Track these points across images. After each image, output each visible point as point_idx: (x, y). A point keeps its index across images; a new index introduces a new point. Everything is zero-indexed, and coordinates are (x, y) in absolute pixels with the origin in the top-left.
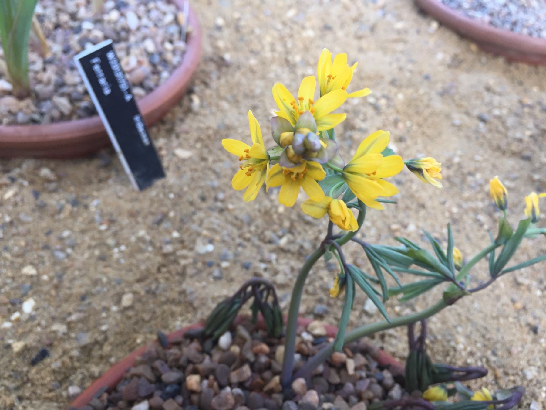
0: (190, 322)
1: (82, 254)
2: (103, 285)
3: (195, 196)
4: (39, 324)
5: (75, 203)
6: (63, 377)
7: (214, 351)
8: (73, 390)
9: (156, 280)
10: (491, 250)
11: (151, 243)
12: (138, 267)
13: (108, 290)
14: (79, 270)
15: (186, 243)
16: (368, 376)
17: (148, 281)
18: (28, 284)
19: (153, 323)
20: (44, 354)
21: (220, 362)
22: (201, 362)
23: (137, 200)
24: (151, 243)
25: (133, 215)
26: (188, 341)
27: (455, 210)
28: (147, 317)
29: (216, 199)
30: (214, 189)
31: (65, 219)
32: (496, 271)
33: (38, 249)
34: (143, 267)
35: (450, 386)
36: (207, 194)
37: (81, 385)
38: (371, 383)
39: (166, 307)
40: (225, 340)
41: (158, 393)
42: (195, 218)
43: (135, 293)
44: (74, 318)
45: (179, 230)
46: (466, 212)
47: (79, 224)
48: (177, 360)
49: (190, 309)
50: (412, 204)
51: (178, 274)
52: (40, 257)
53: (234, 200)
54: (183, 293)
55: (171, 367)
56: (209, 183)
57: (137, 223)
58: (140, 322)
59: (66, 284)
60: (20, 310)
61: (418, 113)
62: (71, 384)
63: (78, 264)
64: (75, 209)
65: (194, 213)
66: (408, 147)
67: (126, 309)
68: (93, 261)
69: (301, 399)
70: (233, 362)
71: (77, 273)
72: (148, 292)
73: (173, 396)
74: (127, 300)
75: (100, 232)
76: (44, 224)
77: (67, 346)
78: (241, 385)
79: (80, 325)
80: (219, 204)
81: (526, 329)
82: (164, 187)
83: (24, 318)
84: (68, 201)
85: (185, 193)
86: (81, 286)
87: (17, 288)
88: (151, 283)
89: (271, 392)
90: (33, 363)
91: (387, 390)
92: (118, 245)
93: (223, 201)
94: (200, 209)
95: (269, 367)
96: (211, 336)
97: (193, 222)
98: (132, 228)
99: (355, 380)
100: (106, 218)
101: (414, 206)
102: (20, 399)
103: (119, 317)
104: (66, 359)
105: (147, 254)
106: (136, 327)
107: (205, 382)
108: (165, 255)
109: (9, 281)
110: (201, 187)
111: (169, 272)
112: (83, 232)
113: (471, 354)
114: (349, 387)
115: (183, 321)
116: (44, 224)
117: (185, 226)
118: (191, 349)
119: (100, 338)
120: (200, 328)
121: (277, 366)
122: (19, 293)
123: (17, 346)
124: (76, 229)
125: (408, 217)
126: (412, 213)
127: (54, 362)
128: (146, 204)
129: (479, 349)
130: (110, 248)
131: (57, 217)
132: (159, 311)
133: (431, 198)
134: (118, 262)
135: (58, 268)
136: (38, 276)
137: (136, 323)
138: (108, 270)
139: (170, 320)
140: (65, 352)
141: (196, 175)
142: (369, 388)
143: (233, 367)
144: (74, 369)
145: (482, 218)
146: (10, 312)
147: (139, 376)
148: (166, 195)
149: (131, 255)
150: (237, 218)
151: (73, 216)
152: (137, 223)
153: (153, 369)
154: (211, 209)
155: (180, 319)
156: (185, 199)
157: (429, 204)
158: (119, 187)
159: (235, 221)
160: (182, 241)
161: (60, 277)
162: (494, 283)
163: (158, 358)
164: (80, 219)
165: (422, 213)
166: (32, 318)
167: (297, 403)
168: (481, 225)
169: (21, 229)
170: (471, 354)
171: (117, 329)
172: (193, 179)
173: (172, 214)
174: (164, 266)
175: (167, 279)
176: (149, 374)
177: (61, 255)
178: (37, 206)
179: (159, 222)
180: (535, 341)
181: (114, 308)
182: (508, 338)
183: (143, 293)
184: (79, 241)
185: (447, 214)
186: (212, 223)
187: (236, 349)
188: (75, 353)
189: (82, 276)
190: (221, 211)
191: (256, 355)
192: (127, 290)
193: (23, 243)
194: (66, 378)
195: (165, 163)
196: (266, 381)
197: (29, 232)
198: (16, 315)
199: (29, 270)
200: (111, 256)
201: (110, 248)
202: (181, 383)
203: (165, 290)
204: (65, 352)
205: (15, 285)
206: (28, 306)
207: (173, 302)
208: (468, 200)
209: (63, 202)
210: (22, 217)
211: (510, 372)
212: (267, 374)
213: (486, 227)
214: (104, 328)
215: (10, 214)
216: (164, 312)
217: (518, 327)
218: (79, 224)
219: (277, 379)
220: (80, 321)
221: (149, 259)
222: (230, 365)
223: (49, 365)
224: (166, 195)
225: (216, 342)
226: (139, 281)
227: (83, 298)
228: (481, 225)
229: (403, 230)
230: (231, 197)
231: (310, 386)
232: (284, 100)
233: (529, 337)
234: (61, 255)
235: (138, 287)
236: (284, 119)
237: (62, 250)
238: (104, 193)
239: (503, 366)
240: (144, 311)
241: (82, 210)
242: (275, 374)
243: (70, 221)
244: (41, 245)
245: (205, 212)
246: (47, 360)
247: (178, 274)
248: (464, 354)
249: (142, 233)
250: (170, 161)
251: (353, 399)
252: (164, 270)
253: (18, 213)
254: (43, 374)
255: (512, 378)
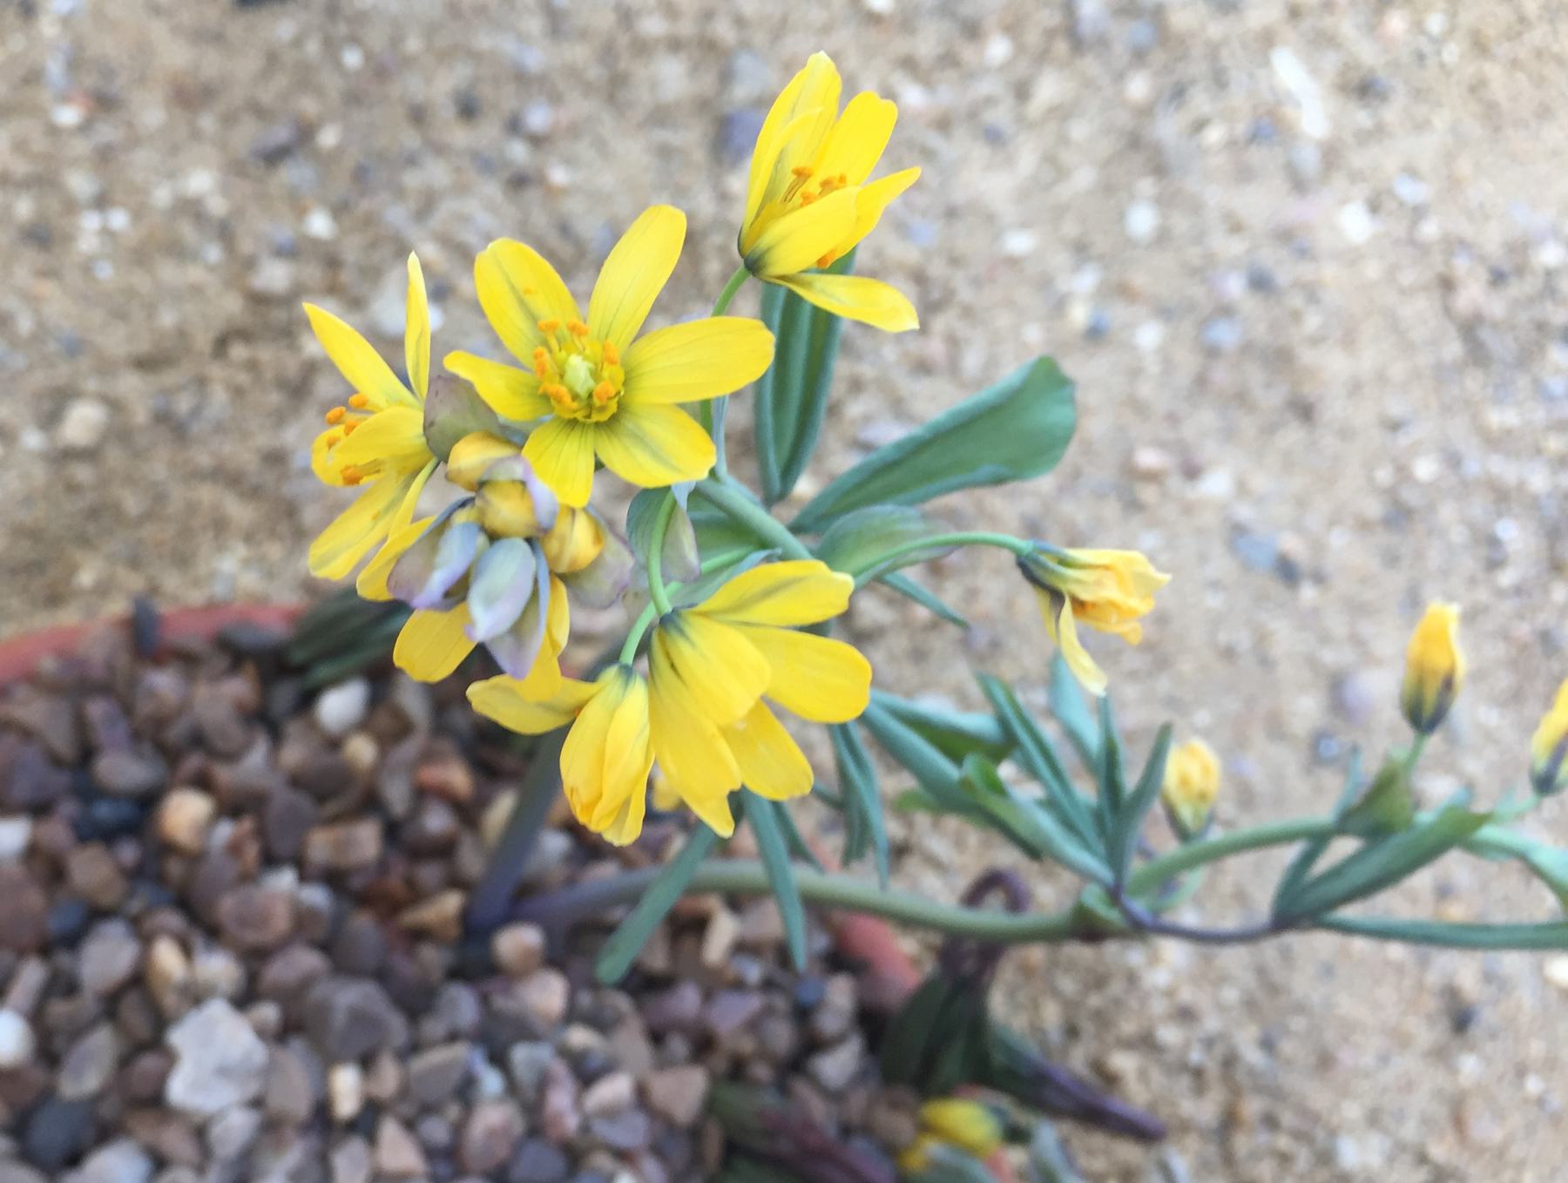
0: (270, 575)
7: (293, 729)
9: (201, 382)
11: (225, 232)
12: (151, 309)
13: (30, 368)
15: (346, 277)
16: (768, 985)
17: (170, 378)
19: (149, 532)
21: (297, 781)
22: (232, 757)
23: (217, 38)
25: (190, 97)
26: (222, 662)
28: (132, 503)
29: (514, 126)
30: (522, 79)
34: (168, 319)
35: (1023, 1117)
36: (486, 91)
38: (768, 1011)
39: (207, 494)
40: (340, 704)
41: (68, 808)
42: (412, 180)
43: (114, 405)
45: (339, 210)
46: (1465, 488)
48: (160, 722)
49: (284, 528)
50: (1268, 386)
51: (282, 383)
53: (583, 149)
54: (276, 458)
55: (136, 736)
56: (508, 46)
57: (196, 135)
58: (101, 516)
65: (412, 161)
66: (1379, 132)
69: (507, 991)
70: (334, 791)
72: (164, 418)
73: (108, 836)
74: (83, 421)
75: (53, 131)
78: (334, 878)
80: (519, 152)
81: (1431, 1003)
85: (408, 62)
88: (181, 388)
89: (419, 935)
91: (812, 1044)
92: (102, 202)
93: (537, 141)
94: (440, 150)
95: (443, 850)
96: (301, 670)
97: (400, 193)
98: (174, 150)
99: (716, 984)
100: (90, 80)
101: (1270, 398)
105: (195, 274)
106: (91, 529)
107: (225, 831)
108: (259, 300)
110: (475, 56)
111: (252, 366)
113: (1186, 1015)
114: (686, 1000)
117: (365, 205)
118: (221, 698)
120: (274, 629)
121: (471, 861)
126: (1248, 425)
128: (246, 66)
129: (1221, 1008)
130: (71, 207)
132: (178, 495)
133: (1355, 388)
134: (87, 268)
137: (94, 513)
138: (47, 288)
142: (754, 1025)
143: (332, 808)
145: (1514, 534)
148: (331, 47)
149: (140, 255)
150: (565, 229)
152: (196, 135)
153: (81, 725)
154: (486, 164)
155: (241, 550)
157: (1334, 408)
159: (553, 240)
163: (103, 689)
165: (1292, 435)
168: (1495, 561)
170: (1186, 1015)
171: (25, 516)
173: (328, 138)
175: (238, 392)
176: (61, 739)
179: (274, 157)
180: (1441, 1055)
181: (33, 439)
182: (1348, 1005)
183: (140, 415)
186: (465, 219)
187: (362, 750)
190: (519, 182)
191: (423, 794)
196: (417, 895)
201: (71, 207)
202: (148, 802)
203: (220, 428)
208: (1496, 442)
211: (1287, 1118)
212: (429, 873)
213: (1506, 578)
216: (191, 509)
217: (1408, 983)
219: (450, 904)
221: (197, 292)
222: (321, 797)
224: (331, 47)
225: (308, 700)
226: (146, 364)
228: (1495, 561)
229: (1175, 483)
231: (556, 958)
233: (1426, 1034)
235: (130, 385)
239: (1276, 1093)
240: (130, 480)
242: (455, 882)
245: (458, 170)
247: (282, 383)
248: (1158, 1007)
249: (201, 181)
251: (678, 1046)
252: (238, 351)
255: (1283, 1142)
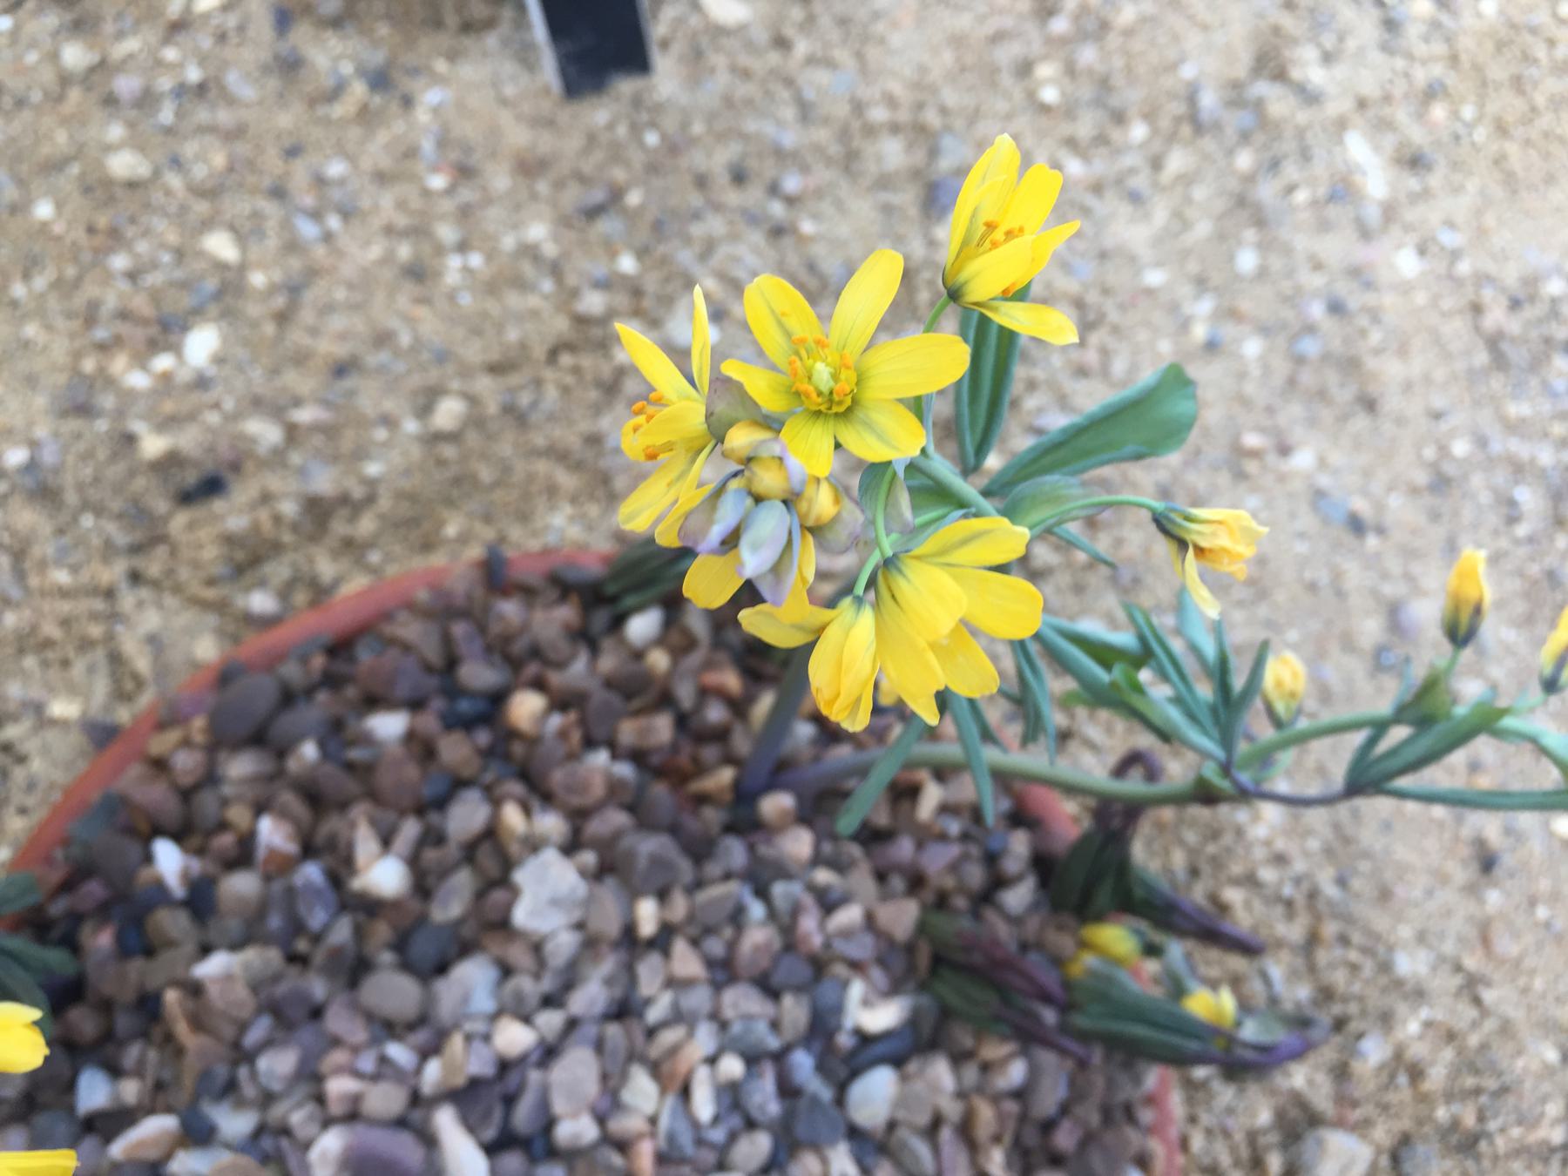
1: (367, 244)
2: (398, 353)
3: (718, 160)
4: (216, 406)
5: (380, 80)
6: (247, 558)
8: (261, 602)
9: (538, 383)
10: (1380, 727)
11: (556, 270)
12: (500, 328)
13: (409, 372)
14: (351, 286)
15: (647, 303)
16: (965, 837)
17: (514, 379)
18: (211, 284)
19: (499, 495)
20: (212, 486)
23: (550, 123)
24: (556, 270)
25: (529, 167)
26: (553, 594)
27: (1461, 448)
28: (486, 474)
29: (774, 190)
31: (343, 122)
32: (1366, 780)
33: (254, 191)
34: (513, 335)
35: (1157, 937)
36: (752, 164)
37: (284, 593)
38: (965, 857)
39: (542, 467)
40: (643, 626)
42: (697, 230)
43: (472, 400)
44: (305, 415)
45: (642, 253)
47: (377, 150)
50: (1342, 385)
52: (256, 215)
53: (826, 207)
54: (594, 440)
56: (768, 129)
57: (534, 197)
59: (307, 316)
60: (176, 349)
61: (1518, 84)
62: (262, 584)
63: (347, 270)
64: (377, 100)
65: (696, 216)
67: (438, 437)
68: (387, 274)
69: (769, 841)
71: (340, 294)
72: (509, 410)
73: (467, 724)
74: (448, 412)
75: (426, 193)
76: (285, 120)
77: (274, 482)
78: (638, 757)
79: (318, 440)
80: (777, 209)
81: (1465, 851)
82: (637, 102)
83: (184, 376)
84: (361, 72)
85: (693, 141)
86: (343, 337)
87: (184, 285)
89: (702, 799)
90: (186, 498)
91: (998, 882)
92: (463, 247)
93: (791, 201)
94: (718, 207)
95: (721, 735)
96: (613, 600)
97: (688, 240)
98: (518, 207)
99: (926, 836)
101: (1344, 395)
102: (135, 578)
103: (416, 452)
104: (264, 515)
105: (533, 301)
108: (581, 321)
109: (166, 258)
111: (576, 370)
112: (382, 178)
113: (1280, 860)
114: (904, 849)
115: (572, 519)
116: (285, 120)
117: (661, 249)
118: (552, 621)
119: (358, 492)
120: (592, 568)
121: (741, 744)
122: (187, 301)
123: (153, 445)
124: (366, 164)
125: (1312, 422)
126: (1327, 415)
127: (234, 513)
128: (572, 144)
129: (1306, 854)
130: (440, 250)
131: (321, 111)
132: (518, 475)
133: (1408, 387)
134: (451, 297)
135: (295, 263)
136: (243, 268)
137: (457, 481)
138: (422, 312)
139: (541, 503)
140: (266, 498)
141: (743, 90)
142: (954, 867)
143: (637, 703)
144: (277, 548)
145: (1528, 497)
146: (155, 346)
147: (406, 648)
148: (636, 130)
149: (492, 287)
150: (812, 267)
151: (365, 115)
152: (534, 197)
153: (447, 640)
156: (684, 162)
157: (1392, 403)
158: (509, 67)
159: (803, 275)
160: (635, 290)
161: (294, 290)
162: (1343, 810)
163: (464, 614)
164: (383, 137)
165: (1361, 422)
166: (201, 382)
167: (751, 848)
169: (224, 117)
170: (1280, 860)
171: (406, 484)
172: (729, 102)
173: (634, 198)
174: (570, 347)
175: (565, 390)
177: (308, 229)
178: (277, 57)
179: (593, 213)
181: (411, 426)
182: (1402, 853)
183: (492, 408)
184: (365, 203)
185: (1429, 453)
186: (737, 260)
187: (659, 660)
188: (289, 508)
189: (355, 307)
190: (778, 232)
191: (704, 693)
192: (455, 385)
193: (219, 160)
194: (255, 561)
195: (659, 27)
196: (700, 770)
197: (236, 134)
198: (163, 362)
199: (221, 246)
200: (438, 274)
201: (440, 250)
202: (498, 698)
203: (552, 418)
204: (266, 498)
205: (179, 274)
206: (202, 344)
207: (559, 454)
208: (1514, 427)
209: (347, 68)
210: (232, 79)
212: (710, 753)
213: (1522, 530)
214: (373, 469)
215: (203, 60)
218: (377, 150)
219: (726, 775)
220: (317, 428)
221: (535, 315)
223: (219, 518)
224: (636, 130)
227: (341, 369)
228: (1513, 519)
229: (1272, 459)
230: (819, 193)
232: (783, 314)
233: (1461, 874)
234: (308, 229)
235: (485, 385)
236: (751, 398)
237: (316, 215)
238: (468, 71)
240: (484, 456)
241: (394, 107)
242: (729, 759)
243: (354, 133)
244: (267, 182)
245: (731, 223)
246: (218, 505)
249: (538, 231)
250: (679, 21)
251: (897, 883)
253: (225, 65)
254: (202, 535)
255: (1353, 956)
